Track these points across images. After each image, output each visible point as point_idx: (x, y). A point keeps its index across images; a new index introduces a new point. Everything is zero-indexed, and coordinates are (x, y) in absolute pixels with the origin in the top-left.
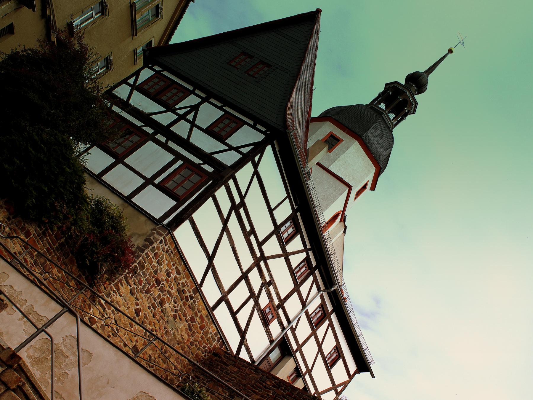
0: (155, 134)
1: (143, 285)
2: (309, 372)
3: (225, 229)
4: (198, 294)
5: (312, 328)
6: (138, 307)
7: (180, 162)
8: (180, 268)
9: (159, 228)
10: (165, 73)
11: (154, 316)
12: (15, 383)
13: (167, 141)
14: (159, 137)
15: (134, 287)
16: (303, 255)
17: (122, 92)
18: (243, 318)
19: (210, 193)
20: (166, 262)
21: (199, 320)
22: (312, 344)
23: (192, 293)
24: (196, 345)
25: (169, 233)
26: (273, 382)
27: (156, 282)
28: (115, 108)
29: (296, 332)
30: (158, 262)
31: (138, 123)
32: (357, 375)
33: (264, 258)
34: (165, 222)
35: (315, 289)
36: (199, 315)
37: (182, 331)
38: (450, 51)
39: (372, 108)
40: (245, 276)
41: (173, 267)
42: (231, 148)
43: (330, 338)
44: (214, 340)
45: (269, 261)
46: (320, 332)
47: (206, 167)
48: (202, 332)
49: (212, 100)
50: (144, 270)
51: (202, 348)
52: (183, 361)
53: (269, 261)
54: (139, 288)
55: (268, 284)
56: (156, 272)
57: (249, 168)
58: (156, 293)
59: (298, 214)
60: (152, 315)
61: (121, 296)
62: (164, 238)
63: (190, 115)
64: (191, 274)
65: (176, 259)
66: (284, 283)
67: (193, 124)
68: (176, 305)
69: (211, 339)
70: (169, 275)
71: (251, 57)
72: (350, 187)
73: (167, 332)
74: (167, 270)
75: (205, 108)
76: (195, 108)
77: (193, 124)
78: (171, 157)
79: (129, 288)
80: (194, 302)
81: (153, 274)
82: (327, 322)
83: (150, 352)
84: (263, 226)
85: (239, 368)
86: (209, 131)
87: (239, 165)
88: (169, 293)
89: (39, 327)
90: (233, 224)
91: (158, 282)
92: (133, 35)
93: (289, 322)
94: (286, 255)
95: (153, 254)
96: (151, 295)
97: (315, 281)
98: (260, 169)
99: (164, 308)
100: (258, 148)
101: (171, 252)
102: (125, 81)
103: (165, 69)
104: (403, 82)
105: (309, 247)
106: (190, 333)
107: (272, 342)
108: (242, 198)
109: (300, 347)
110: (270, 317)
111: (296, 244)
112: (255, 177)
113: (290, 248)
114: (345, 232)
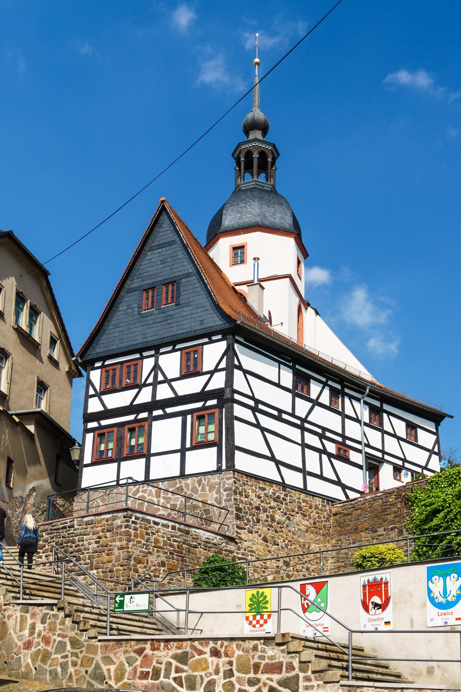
0: (150, 413)
1: (251, 520)
2: (404, 460)
3: (263, 430)
4: (288, 489)
6: (262, 536)
8: (261, 485)
9: (224, 475)
10: (107, 363)
11: (276, 532)
12: (299, 647)
13: (164, 411)
14: (156, 413)
15: (248, 528)
17: (94, 406)
18: (328, 473)
19: (232, 418)
20: (250, 491)
23: (284, 493)
24: (318, 522)
25: (234, 471)
26: (393, 496)
27: (257, 510)
28: (104, 423)
29: (371, 444)
30: (246, 497)
31: (131, 417)
32: (439, 427)
33: (304, 420)
34: (224, 467)
35: (355, 403)
36: (301, 501)
37: (301, 522)
40: (304, 446)
41: (257, 490)
42: (211, 373)
45: (309, 419)
46: (387, 427)
48: (313, 509)
49: (162, 350)
50: (243, 510)
51: (323, 519)
52: (320, 540)
53: (309, 419)
54: (251, 525)
56: (251, 504)
57: (238, 374)
58: (263, 516)
59: (297, 367)
60: (274, 532)
61: (246, 541)
62: (234, 478)
63: (158, 377)
66: (331, 421)
67: (167, 381)
68: (282, 510)
69: (323, 508)
70: (259, 497)
73: (293, 533)
74: (256, 495)
75: (164, 360)
76: (156, 368)
77: (167, 381)
78: (179, 419)
79: (246, 530)
80: (290, 496)
81: (250, 507)
84: (283, 400)
85: (361, 509)
87: (229, 380)
88: (271, 508)
89: (277, 610)
90: (265, 421)
91: (258, 508)
93: (360, 443)
94: (316, 403)
95: (238, 495)
96: (262, 520)
99: (277, 520)
101: (247, 481)
102: (88, 396)
103: (104, 359)
105: (324, 380)
106: (307, 518)
107: (360, 467)
108: (252, 398)
112: (247, 375)
113: (313, 396)
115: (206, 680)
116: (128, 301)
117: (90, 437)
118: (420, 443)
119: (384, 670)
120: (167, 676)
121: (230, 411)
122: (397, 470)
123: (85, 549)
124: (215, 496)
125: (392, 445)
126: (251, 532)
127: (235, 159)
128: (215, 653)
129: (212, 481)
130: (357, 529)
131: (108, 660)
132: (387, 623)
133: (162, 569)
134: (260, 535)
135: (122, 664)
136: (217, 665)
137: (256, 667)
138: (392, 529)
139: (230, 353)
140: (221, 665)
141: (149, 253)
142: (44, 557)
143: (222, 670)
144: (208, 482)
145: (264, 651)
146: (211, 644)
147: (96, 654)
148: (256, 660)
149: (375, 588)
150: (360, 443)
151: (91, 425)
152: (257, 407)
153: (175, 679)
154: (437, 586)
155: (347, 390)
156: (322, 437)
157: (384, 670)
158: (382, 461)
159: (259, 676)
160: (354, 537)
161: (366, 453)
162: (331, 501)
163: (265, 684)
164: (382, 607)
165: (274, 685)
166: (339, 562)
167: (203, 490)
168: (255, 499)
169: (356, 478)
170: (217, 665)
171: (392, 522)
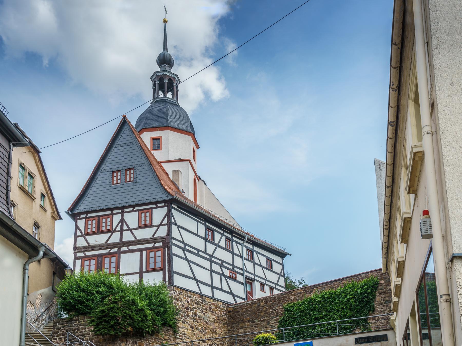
0: (119, 249)
2: (266, 280)
3: (189, 261)
5: (252, 262)
7: (144, 253)
8: (189, 295)
11: (198, 322)
16: (224, 237)
18: (225, 288)
19: (170, 255)
20: (183, 298)
21: (213, 306)
22: (258, 269)
33: (212, 256)
34: (167, 284)
38: (165, 22)
39: (157, 102)
40: (212, 271)
42: (159, 226)
43: (261, 258)
44: (224, 307)
46: (256, 260)
47: (157, 245)
49: (126, 210)
55: (222, 264)
56: (183, 306)
57: (174, 228)
58: (190, 313)
64: (194, 293)
65: (184, 293)
66: (226, 256)
67: (129, 229)
70: (188, 302)
71: (119, 171)
72: (188, 160)
75: (127, 217)
77: (129, 229)
80: (205, 301)
82: (255, 253)
83: (209, 336)
84: (199, 244)
85: (245, 309)
86: (141, 227)
87: (169, 231)
88: (194, 308)
90: (191, 257)
91: (187, 308)
92: (33, 200)
93: (242, 269)
94: (218, 246)
97: (237, 242)
98: (178, 224)
103: (87, 213)
104: (158, 69)
105: (222, 232)
107: (243, 284)
108: (183, 242)
109: (254, 274)
110: (234, 276)
111: (217, 236)
113: (216, 241)
114: (205, 184)
116: (102, 177)
117: (78, 262)
121: (170, 250)
122: (262, 285)
123: (87, 334)
126: (184, 323)
127: (152, 81)
130: (243, 320)
134: (189, 325)
138: (263, 321)
139: (169, 215)
141: (115, 149)
142: (58, 339)
150: (263, 279)
151: (79, 255)
152: (185, 247)
155: (234, 239)
156: (221, 266)
158: (254, 280)
160: (241, 325)
162: (227, 304)
168: (186, 303)
169: (239, 290)
171: (263, 317)
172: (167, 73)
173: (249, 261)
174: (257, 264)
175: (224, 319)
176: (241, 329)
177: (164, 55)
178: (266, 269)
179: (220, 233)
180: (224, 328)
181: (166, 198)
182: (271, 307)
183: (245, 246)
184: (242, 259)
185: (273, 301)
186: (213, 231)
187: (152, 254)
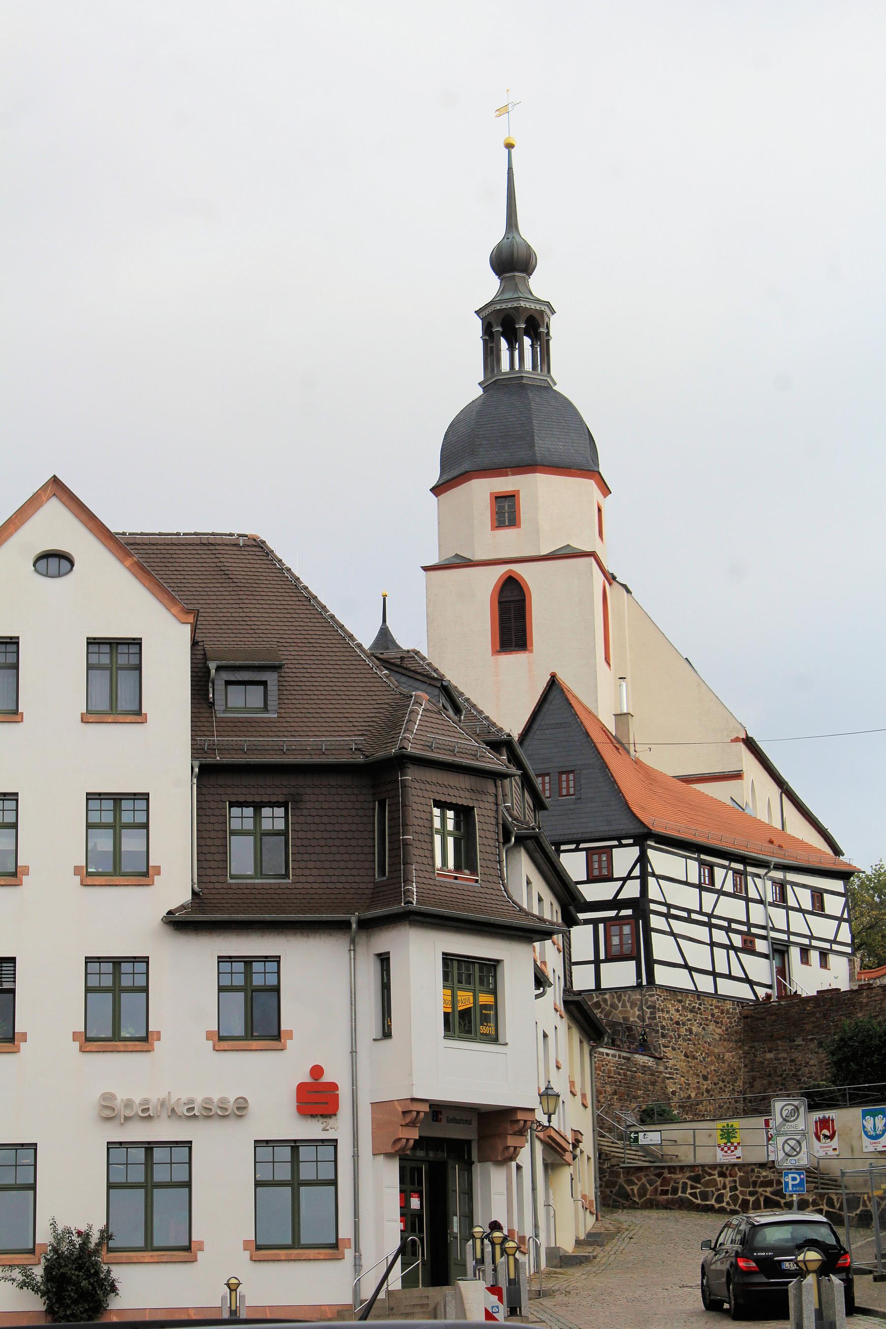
2: (811, 937)
5: (783, 907)
7: (601, 926)
11: (695, 1045)
16: (730, 872)
19: (648, 930)
33: (710, 916)
34: (644, 983)
38: (509, 146)
42: (624, 880)
44: (735, 1009)
47: (624, 913)
49: (563, 847)
57: (651, 881)
70: (678, 1011)
82: (789, 887)
84: (687, 898)
88: (689, 1020)
91: (677, 1023)
93: (764, 928)
94: (721, 893)
98: (657, 873)
100: (643, 860)
107: (766, 956)
111: (719, 873)
115: (716, 1194)
118: (827, 912)
119: (835, 1183)
120: (684, 1192)
124: (637, 1013)
125: (798, 923)
126: (674, 1049)
128: (722, 1175)
129: (633, 997)
130: (772, 1036)
131: (630, 1183)
132: (835, 1149)
133: (616, 1097)
135: (643, 1185)
136: (724, 1183)
137: (755, 1184)
138: (811, 1040)
139: (643, 860)
140: (727, 1183)
141: (538, 732)
143: (728, 1186)
144: (629, 998)
145: (759, 1172)
146: (719, 1169)
147: (618, 1177)
148: (754, 1179)
149: (824, 1123)
153: (690, 1194)
154: (869, 1122)
156: (728, 930)
157: (835, 1183)
159: (757, 1189)
160: (770, 1045)
161: (773, 938)
162: (740, 1002)
163: (762, 1195)
164: (831, 1137)
165: (768, 1194)
166: (753, 1071)
167: (624, 1006)
169: (760, 969)
170: (724, 1183)
172: (522, 304)
173: (778, 906)
174: (793, 909)
175: (736, 1032)
176: (770, 1051)
177: (511, 246)
178: (811, 913)
179: (723, 867)
180: (736, 1049)
181: (637, 831)
182: (825, 1016)
183: (771, 879)
184: (765, 907)
185: (829, 1004)
186: (711, 866)
187: (615, 930)
